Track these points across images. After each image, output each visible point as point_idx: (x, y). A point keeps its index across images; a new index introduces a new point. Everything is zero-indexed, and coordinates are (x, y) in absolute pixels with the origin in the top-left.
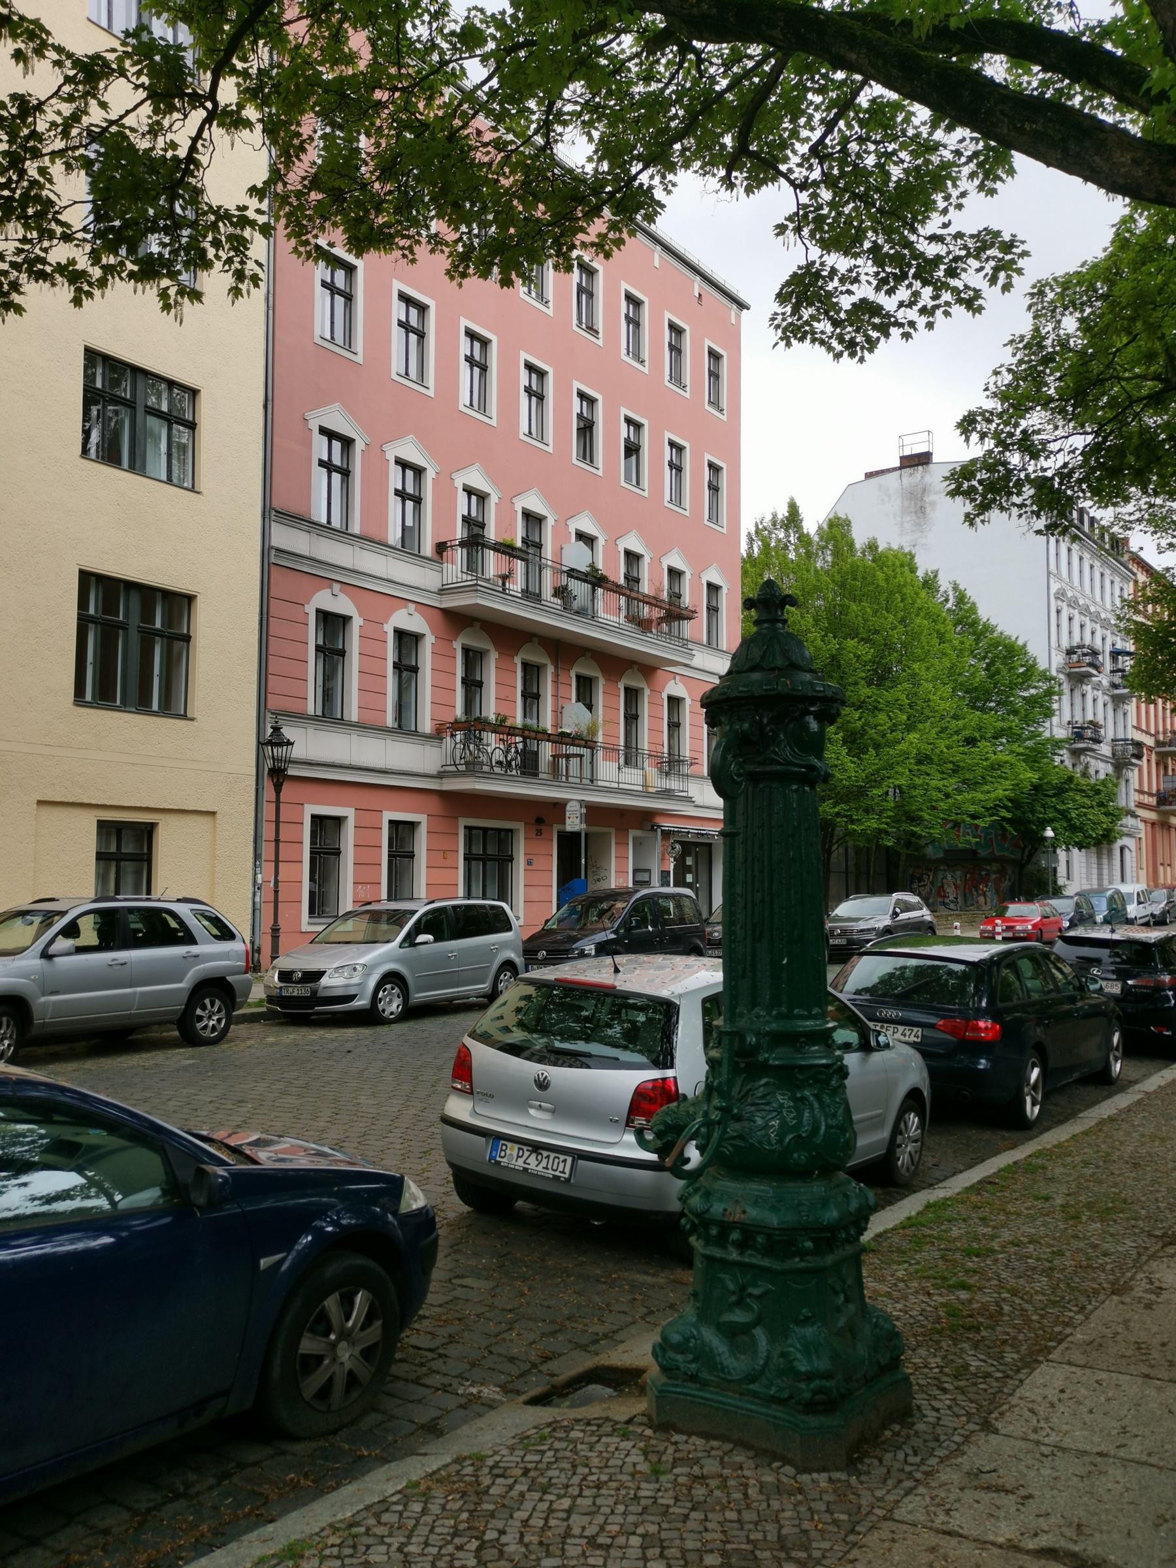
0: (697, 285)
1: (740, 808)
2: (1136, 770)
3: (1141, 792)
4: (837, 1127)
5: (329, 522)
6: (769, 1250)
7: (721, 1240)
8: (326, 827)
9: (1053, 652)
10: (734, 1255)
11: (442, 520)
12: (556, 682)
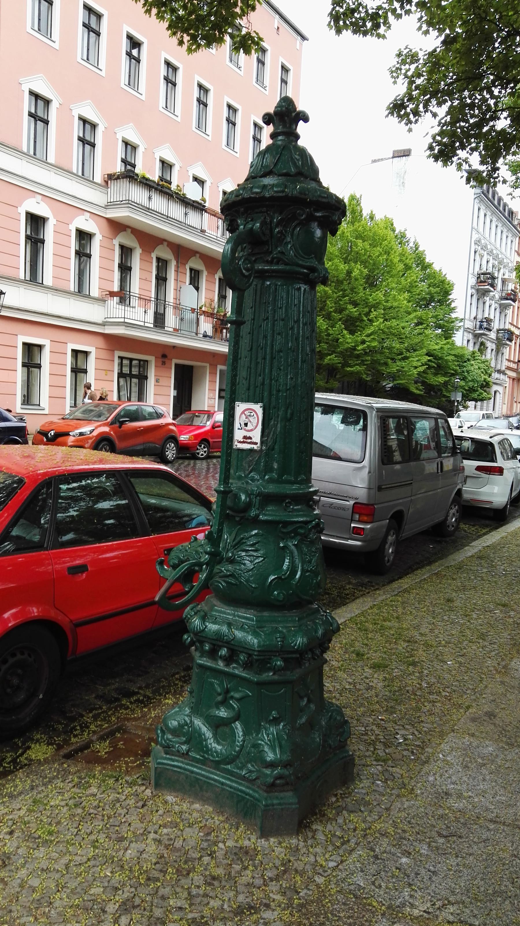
0: (277, 21)
1: (248, 300)
2: (508, 349)
3: (509, 361)
4: (311, 571)
5: (35, 154)
6: (247, 666)
7: (213, 654)
8: (31, 350)
9: (470, 276)
10: (221, 665)
11: (107, 159)
12: (177, 271)
